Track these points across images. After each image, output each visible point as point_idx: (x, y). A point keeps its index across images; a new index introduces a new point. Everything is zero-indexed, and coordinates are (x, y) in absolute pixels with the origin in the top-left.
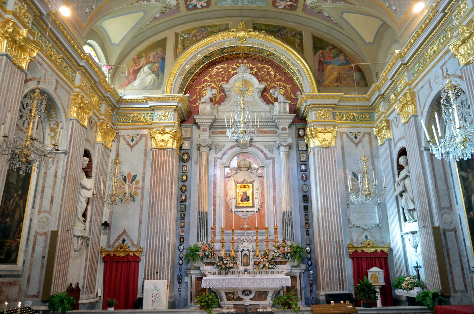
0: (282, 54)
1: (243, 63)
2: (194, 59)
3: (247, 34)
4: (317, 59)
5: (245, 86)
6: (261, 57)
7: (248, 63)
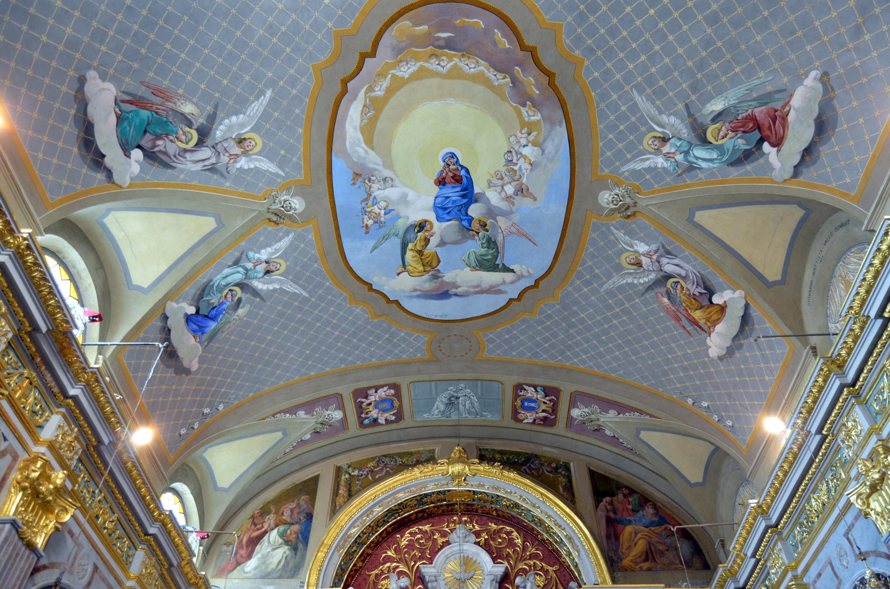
0: (534, 506)
1: (460, 522)
2: (368, 516)
3: (467, 469)
4: (601, 513)
5: (465, 570)
6: (496, 510)
7: (471, 522)
